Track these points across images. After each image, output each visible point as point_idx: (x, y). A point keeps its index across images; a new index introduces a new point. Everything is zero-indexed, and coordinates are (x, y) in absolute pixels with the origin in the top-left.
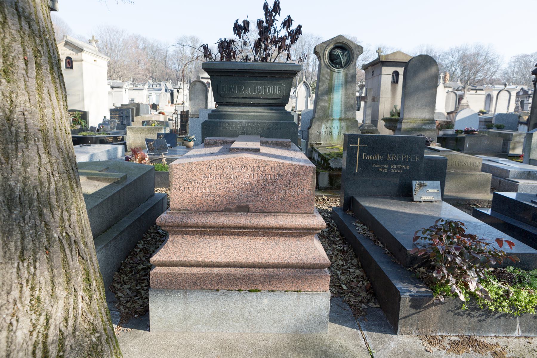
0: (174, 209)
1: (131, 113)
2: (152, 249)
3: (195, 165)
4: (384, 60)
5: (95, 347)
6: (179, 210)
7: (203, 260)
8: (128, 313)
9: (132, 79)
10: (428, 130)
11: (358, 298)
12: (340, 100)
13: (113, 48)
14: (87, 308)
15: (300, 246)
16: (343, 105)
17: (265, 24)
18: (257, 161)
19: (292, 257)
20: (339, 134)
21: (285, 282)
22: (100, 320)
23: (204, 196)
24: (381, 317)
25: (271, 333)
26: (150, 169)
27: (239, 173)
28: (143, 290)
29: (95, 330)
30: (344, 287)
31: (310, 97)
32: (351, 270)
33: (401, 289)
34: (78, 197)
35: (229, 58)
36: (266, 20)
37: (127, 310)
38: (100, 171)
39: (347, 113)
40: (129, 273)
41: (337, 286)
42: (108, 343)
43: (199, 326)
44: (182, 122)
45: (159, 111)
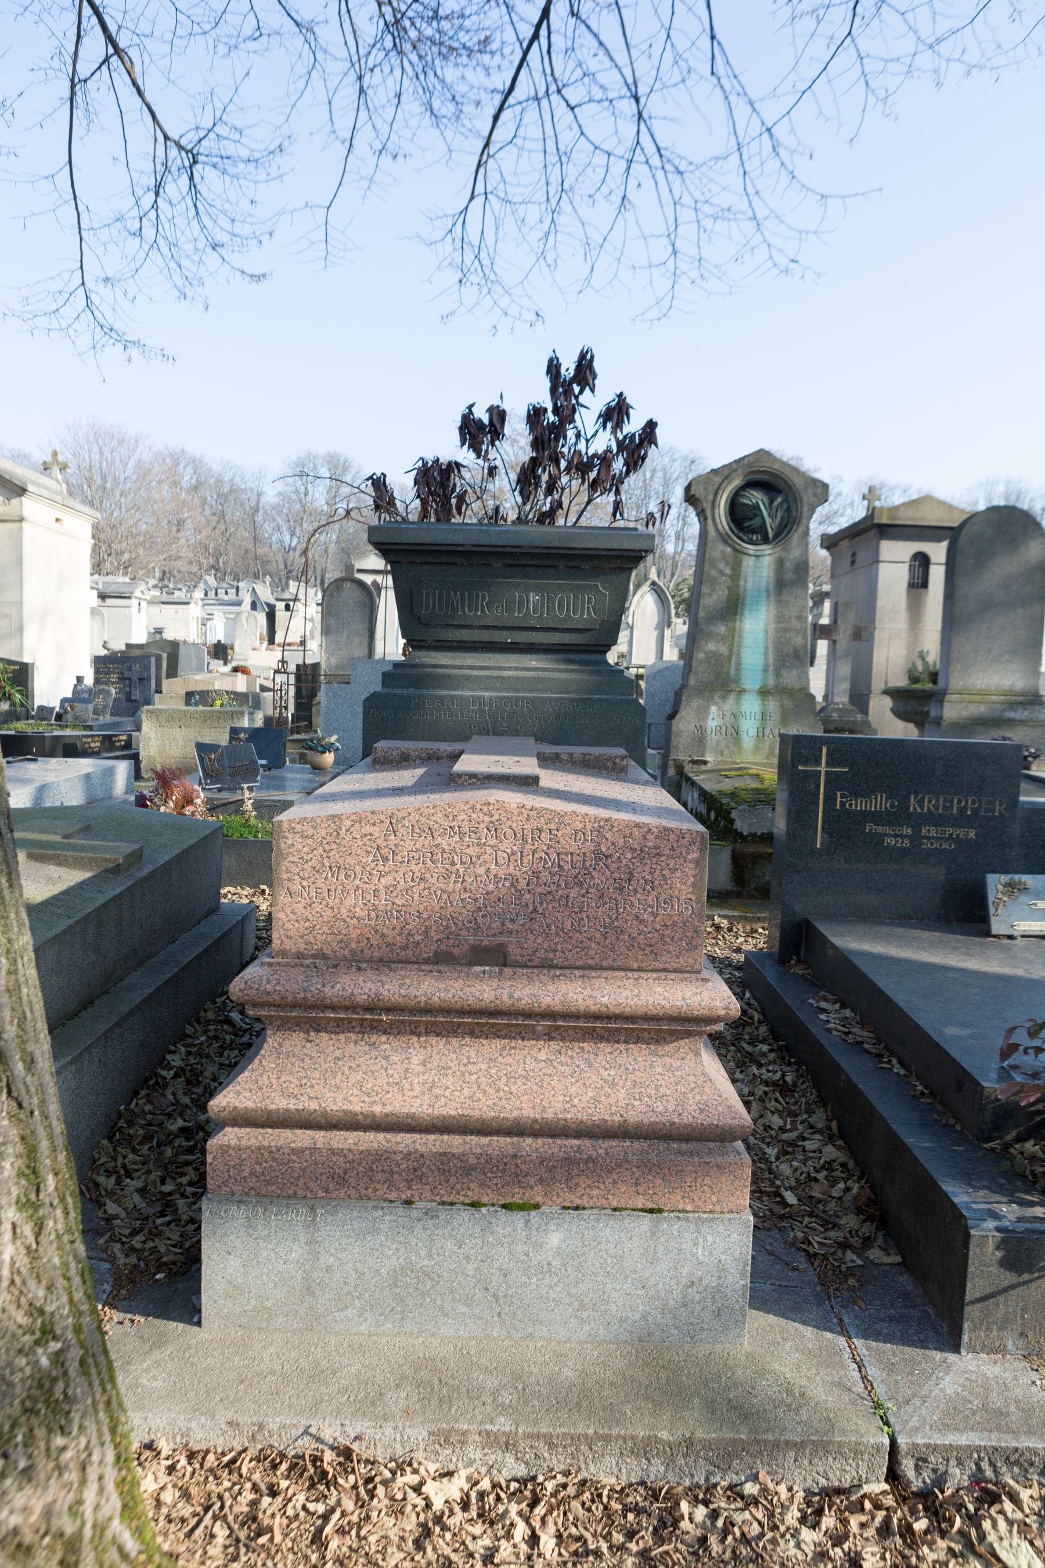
0: (284, 953)
1: (153, 669)
2: (211, 1069)
3: (347, 823)
4: (884, 520)
5: (47, 1384)
6: (300, 956)
7: (366, 1108)
8: (136, 1266)
9: (158, 574)
10: (1022, 723)
11: (832, 1234)
12: (762, 636)
13: (109, 485)
14: (26, 1260)
15: (659, 1070)
16: (771, 650)
17: (551, 417)
18: (534, 813)
19: (636, 1103)
20: (761, 736)
21: (614, 1183)
22: (65, 1298)
23: (373, 915)
24: (906, 1296)
25: (569, 1340)
26: (208, 831)
27: (477, 849)
28: (183, 1195)
29: (48, 1333)
30: (790, 1198)
31: (669, 626)
32: (810, 1145)
33: (969, 1209)
34: (12, 916)
35: (445, 513)
36: (555, 405)
37: (133, 1259)
38: (65, 837)
39: (784, 672)
40: (141, 1143)
41: (768, 1194)
42: (86, 1374)
43: (351, 1313)
44: (298, 695)
45: (234, 664)
